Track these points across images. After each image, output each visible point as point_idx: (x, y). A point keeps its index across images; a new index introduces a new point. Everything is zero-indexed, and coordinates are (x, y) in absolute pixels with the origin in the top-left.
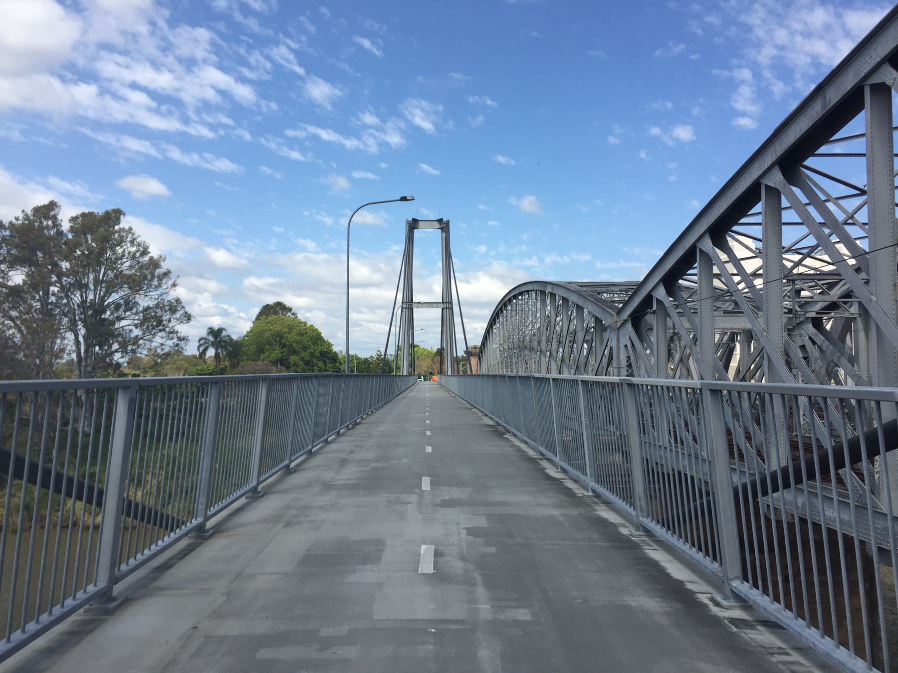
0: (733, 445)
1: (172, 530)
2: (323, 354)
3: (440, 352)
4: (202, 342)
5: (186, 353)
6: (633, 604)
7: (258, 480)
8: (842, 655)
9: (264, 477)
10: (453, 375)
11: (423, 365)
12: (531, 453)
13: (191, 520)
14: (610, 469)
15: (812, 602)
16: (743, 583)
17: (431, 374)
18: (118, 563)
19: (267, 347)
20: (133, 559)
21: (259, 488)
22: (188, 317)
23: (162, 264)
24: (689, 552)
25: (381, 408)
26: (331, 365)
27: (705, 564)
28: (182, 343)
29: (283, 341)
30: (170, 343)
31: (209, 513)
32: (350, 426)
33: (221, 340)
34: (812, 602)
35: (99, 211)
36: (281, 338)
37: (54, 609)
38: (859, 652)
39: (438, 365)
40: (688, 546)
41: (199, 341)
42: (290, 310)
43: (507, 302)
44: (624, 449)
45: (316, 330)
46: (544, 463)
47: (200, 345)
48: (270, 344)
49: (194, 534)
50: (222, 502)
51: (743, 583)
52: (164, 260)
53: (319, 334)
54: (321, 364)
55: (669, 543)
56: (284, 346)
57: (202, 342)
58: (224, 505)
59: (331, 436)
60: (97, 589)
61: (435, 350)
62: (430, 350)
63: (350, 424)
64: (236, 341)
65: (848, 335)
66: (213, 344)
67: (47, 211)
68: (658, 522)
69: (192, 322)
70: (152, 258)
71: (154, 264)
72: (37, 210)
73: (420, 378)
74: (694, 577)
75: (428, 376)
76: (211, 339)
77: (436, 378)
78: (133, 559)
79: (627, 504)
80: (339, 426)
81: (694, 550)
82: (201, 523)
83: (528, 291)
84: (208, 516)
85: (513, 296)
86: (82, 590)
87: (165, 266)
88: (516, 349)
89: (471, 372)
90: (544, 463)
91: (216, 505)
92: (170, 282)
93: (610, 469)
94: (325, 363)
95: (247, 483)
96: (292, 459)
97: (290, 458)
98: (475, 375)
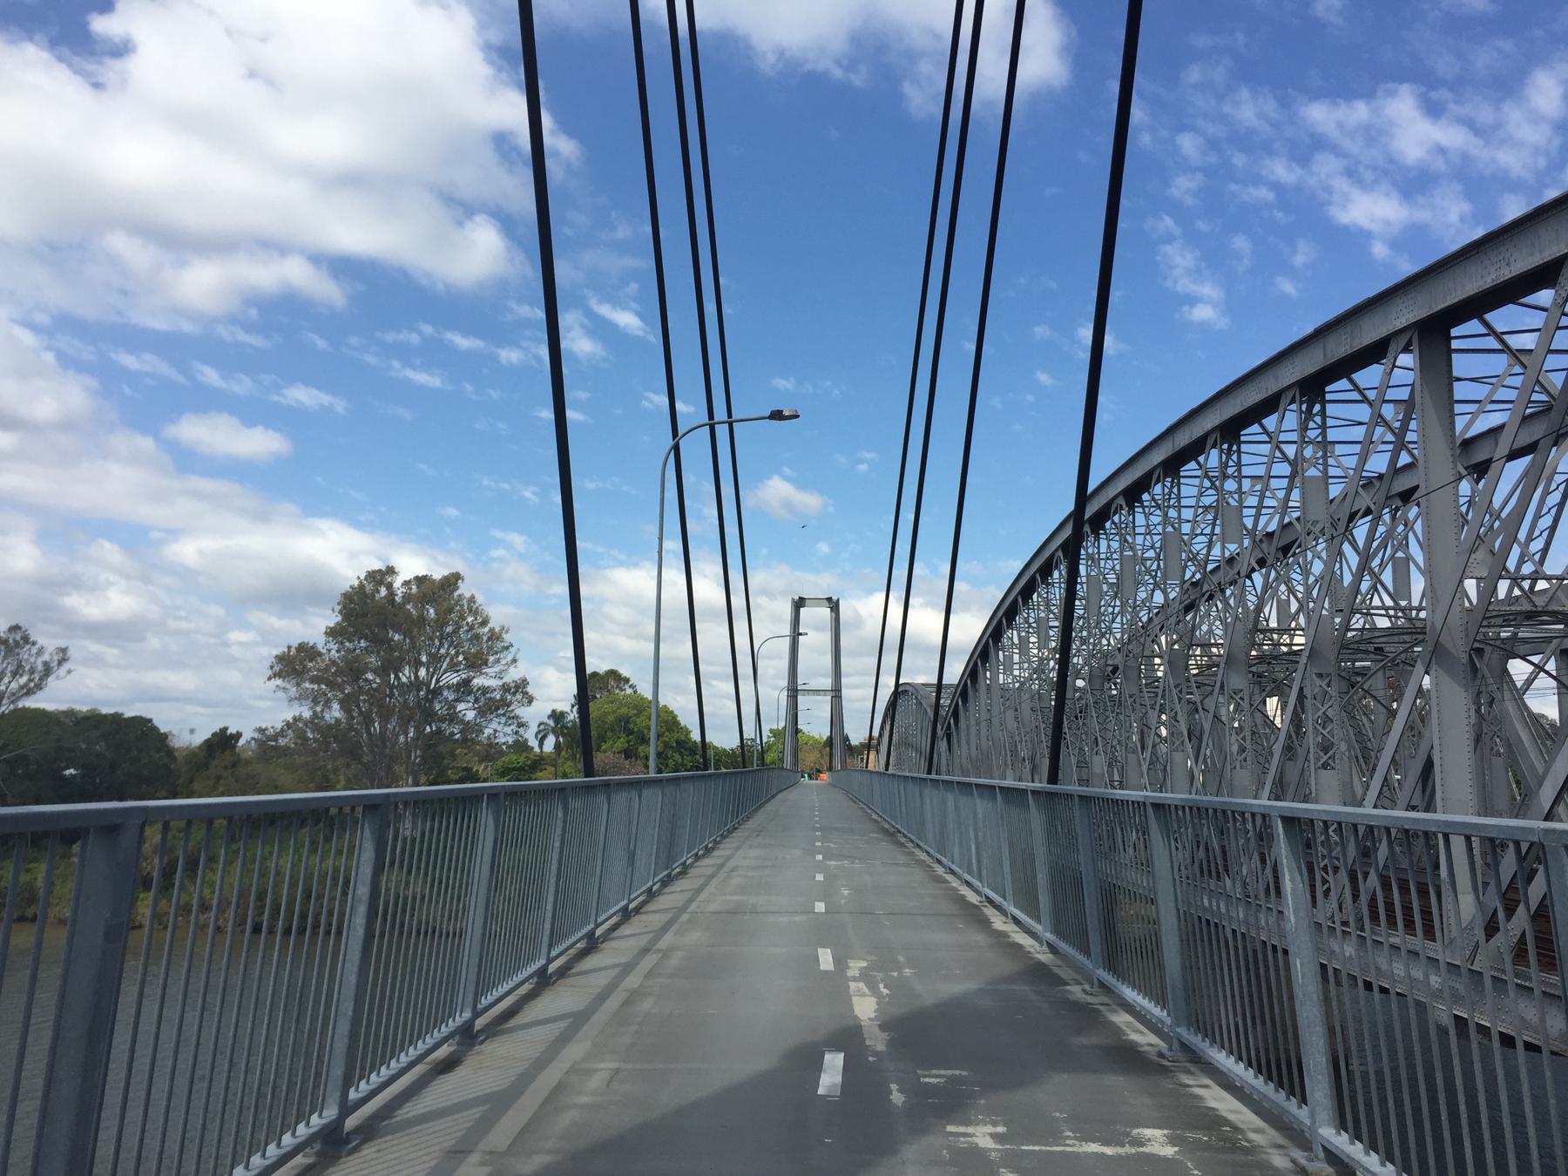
0: (1395, 917)
1: (410, 1044)
2: (678, 743)
3: (830, 739)
4: (542, 727)
7: (548, 956)
8: (1372, 1161)
9: (490, 999)
10: (1435, 834)
11: (809, 759)
12: (973, 898)
15: (1371, 1124)
16: (1340, 1134)
17: (819, 771)
18: (263, 1144)
19: (609, 734)
20: (242, 1166)
21: (598, 932)
22: (531, 700)
23: (504, 636)
24: (1286, 1104)
25: (726, 837)
26: (689, 758)
27: (1238, 1072)
28: (521, 730)
29: (631, 726)
30: (508, 730)
31: (479, 1006)
33: (563, 727)
34: (1371, 1124)
35: (438, 574)
36: (627, 722)
37: (284, 1137)
38: (1389, 1157)
39: (827, 759)
40: (1282, 1094)
42: (627, 680)
45: (672, 712)
46: (990, 912)
48: (613, 730)
49: (535, 980)
50: (447, 1025)
51: (1340, 1134)
52: (507, 632)
53: (675, 717)
54: (677, 757)
55: (1233, 1076)
56: (631, 732)
57: (542, 727)
58: (494, 998)
60: (323, 1121)
61: (825, 738)
66: (554, 731)
67: (381, 577)
68: (1241, 1059)
69: (535, 703)
70: (492, 630)
71: (494, 637)
72: (372, 575)
73: (803, 777)
74: (1258, 1122)
75: (814, 773)
76: (551, 723)
77: (825, 776)
78: (242, 1166)
79: (1203, 1040)
81: (1242, 1065)
82: (466, 1022)
84: (349, 1104)
86: (259, 1154)
87: (507, 637)
89: (867, 767)
90: (990, 912)
91: (420, 1042)
92: (510, 657)
94: (681, 754)
95: (452, 1015)
96: (599, 920)
97: (549, 952)
98: (871, 772)
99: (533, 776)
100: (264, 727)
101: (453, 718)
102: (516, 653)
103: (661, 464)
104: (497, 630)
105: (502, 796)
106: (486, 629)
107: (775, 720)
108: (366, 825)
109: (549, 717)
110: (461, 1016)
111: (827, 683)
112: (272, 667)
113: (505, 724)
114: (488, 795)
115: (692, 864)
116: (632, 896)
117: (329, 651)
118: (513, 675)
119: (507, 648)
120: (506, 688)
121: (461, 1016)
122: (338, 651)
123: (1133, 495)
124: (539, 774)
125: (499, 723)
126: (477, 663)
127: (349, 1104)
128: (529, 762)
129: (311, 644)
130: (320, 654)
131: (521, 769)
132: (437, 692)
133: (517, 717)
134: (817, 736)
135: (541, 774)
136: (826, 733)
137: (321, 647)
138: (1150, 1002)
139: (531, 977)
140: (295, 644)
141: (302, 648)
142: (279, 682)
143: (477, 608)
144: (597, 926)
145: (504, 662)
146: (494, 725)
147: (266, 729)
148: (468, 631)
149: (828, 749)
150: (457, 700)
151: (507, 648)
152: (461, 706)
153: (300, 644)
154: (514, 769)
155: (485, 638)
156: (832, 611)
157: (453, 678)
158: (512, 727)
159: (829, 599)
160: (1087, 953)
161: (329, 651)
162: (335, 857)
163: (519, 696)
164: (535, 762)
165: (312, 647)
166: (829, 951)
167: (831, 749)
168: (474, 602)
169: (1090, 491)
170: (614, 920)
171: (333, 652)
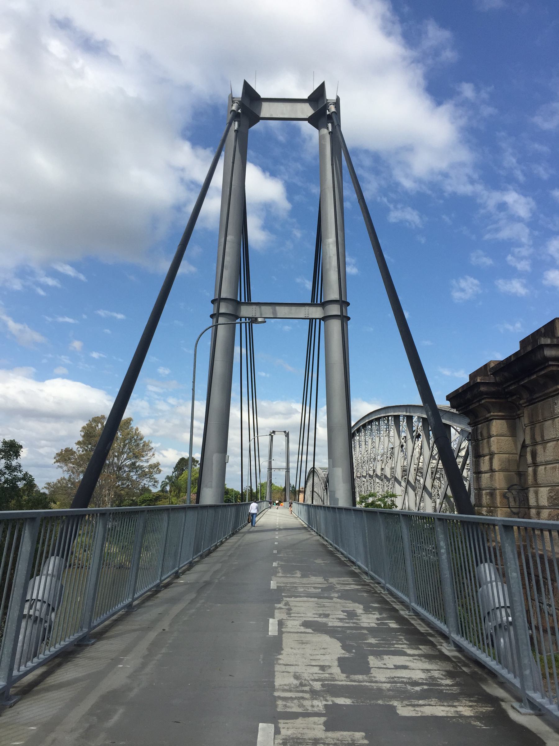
5: (189, 456)
6: (393, 613)
13: (100, 616)
14: (426, 566)
21: (180, 571)
22: (160, 471)
32: (228, 537)
41: (162, 482)
43: (356, 432)
44: (458, 555)
47: (162, 485)
52: (151, 443)
57: (163, 483)
59: (195, 558)
62: (280, 487)
63: (228, 536)
64: (7, 683)
65: (395, 622)
80: (217, 541)
83: (378, 419)
85: (362, 425)
88: (365, 477)
93: (426, 566)
97: (134, 595)
99: (156, 504)
100: (49, 482)
101: (128, 478)
102: (154, 451)
103: (200, 334)
104: (147, 442)
105: (171, 509)
106: (142, 442)
107: (264, 480)
108: (101, 521)
109: (166, 479)
110: (128, 600)
111: (284, 465)
112: (55, 458)
113: (149, 482)
114: (100, 514)
115: (225, 541)
116: (181, 566)
117: (79, 451)
118: (153, 461)
119: (151, 449)
120: (151, 467)
121: (128, 600)
122: (83, 452)
123: (359, 430)
124: (159, 502)
125: (147, 481)
126: (137, 456)
127: (134, 598)
128: (154, 497)
129: (71, 448)
130: (75, 452)
131: (151, 500)
132: (120, 468)
133: (154, 478)
134: (280, 487)
135: (160, 502)
136: (283, 486)
137: (75, 450)
138: (441, 622)
139: (173, 574)
140: (64, 449)
141: (67, 450)
142: (58, 464)
143: (139, 433)
144: (180, 569)
145: (149, 455)
146: (145, 482)
147: (50, 483)
148: (134, 442)
149: (284, 492)
150: (130, 471)
151: (151, 449)
152: (132, 474)
153: (66, 449)
154: (148, 500)
155: (141, 445)
156: (286, 436)
157: (128, 462)
158: (152, 483)
159: (285, 432)
160: (408, 595)
161: (79, 451)
162: (78, 537)
163: (155, 469)
164: (157, 497)
165: (71, 450)
166: (273, 725)
167: (285, 492)
168: (138, 430)
169: (352, 426)
170: (186, 567)
171: (81, 452)
